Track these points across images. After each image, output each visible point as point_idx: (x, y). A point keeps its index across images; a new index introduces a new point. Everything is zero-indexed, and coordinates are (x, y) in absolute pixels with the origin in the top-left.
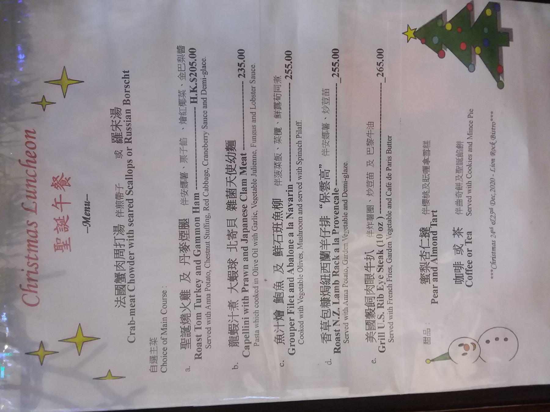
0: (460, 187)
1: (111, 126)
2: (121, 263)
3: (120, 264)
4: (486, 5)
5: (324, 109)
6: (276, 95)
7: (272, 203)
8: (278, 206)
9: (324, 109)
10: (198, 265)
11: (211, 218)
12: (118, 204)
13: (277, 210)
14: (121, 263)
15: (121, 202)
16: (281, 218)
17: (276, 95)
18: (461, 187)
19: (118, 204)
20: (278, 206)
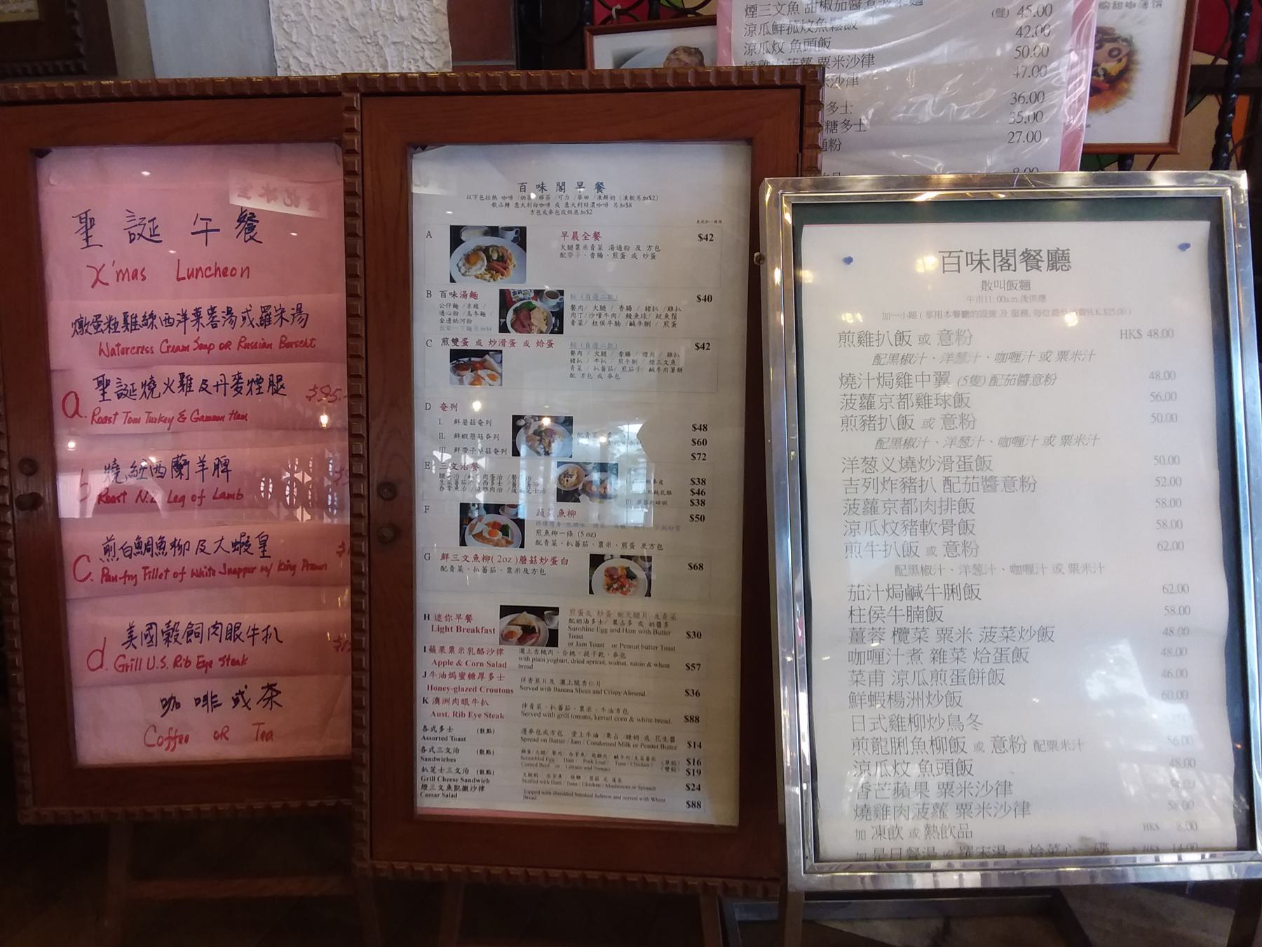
0: (976, 679)
1: (193, 391)
2: (933, 508)
3: (930, 507)
4: (521, 226)
5: (1029, 632)
6: (976, 480)
7: (939, 737)
8: (913, 725)
9: (1029, 632)
10: (1167, 460)
11: (1181, 461)
12: (855, 547)
13: (928, 744)
14: (933, 508)
15: (859, 553)
16: (915, 751)
17: (976, 480)
18: (976, 681)
19: (855, 547)
20: (913, 725)
